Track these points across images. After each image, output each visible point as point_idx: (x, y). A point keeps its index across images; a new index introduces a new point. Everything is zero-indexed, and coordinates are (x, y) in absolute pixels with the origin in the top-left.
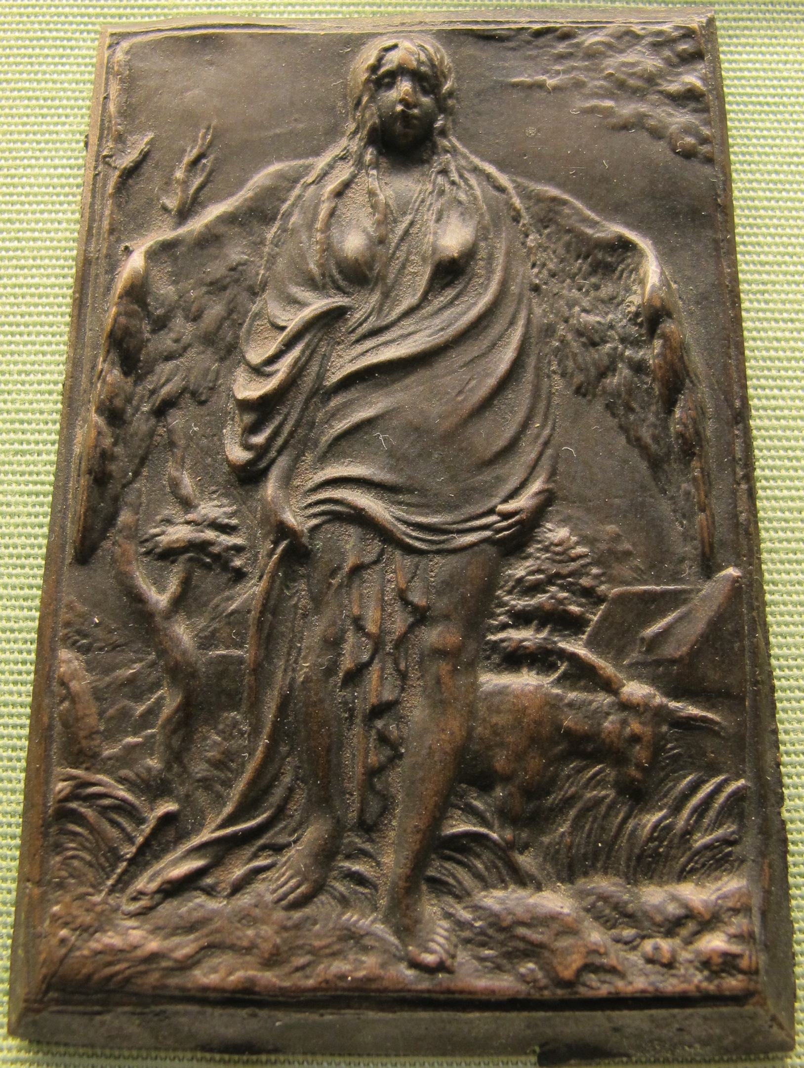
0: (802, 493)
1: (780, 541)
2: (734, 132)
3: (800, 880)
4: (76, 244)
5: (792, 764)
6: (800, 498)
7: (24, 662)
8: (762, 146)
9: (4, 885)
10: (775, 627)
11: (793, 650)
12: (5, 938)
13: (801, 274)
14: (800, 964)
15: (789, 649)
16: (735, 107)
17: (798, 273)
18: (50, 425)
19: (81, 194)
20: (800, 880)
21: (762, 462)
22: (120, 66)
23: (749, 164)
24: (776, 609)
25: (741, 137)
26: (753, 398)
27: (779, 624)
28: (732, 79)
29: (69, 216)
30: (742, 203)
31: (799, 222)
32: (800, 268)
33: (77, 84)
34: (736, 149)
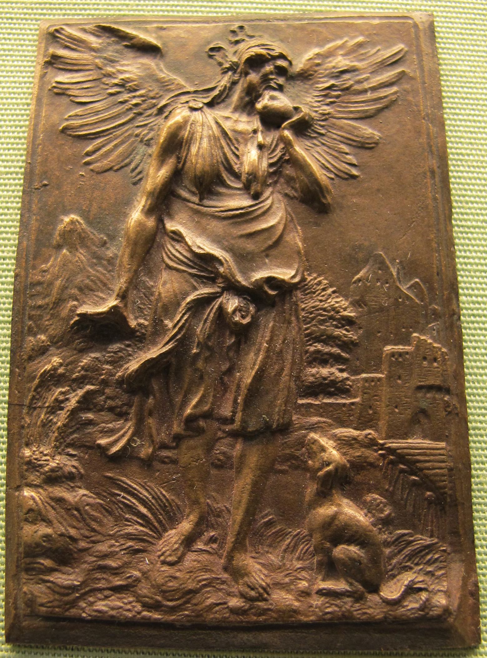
0: (485, 312)
1: (479, 416)
2: (464, 311)
3: (484, 571)
4: (26, 141)
5: (480, 504)
6: (485, 316)
7: (13, 221)
8: (481, 284)
9: (2, 379)
10: (481, 563)
11: (476, 384)
12: (2, 508)
13: (485, 139)
14: (483, 647)
15: (474, 383)
16: (455, 174)
17: (483, 139)
18: (16, 193)
19: (14, 271)
20: (484, 571)
21: (462, 285)
22: (18, 497)
23: (472, 310)
24: (480, 522)
25: (454, 137)
26: (446, 120)
27: (478, 463)
28: (468, 323)
29: (15, 205)
30: (457, 198)
31: (484, 108)
32: (484, 136)
33: (4, 259)
34: (447, 100)
